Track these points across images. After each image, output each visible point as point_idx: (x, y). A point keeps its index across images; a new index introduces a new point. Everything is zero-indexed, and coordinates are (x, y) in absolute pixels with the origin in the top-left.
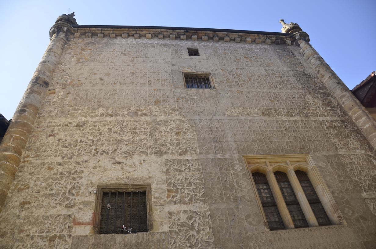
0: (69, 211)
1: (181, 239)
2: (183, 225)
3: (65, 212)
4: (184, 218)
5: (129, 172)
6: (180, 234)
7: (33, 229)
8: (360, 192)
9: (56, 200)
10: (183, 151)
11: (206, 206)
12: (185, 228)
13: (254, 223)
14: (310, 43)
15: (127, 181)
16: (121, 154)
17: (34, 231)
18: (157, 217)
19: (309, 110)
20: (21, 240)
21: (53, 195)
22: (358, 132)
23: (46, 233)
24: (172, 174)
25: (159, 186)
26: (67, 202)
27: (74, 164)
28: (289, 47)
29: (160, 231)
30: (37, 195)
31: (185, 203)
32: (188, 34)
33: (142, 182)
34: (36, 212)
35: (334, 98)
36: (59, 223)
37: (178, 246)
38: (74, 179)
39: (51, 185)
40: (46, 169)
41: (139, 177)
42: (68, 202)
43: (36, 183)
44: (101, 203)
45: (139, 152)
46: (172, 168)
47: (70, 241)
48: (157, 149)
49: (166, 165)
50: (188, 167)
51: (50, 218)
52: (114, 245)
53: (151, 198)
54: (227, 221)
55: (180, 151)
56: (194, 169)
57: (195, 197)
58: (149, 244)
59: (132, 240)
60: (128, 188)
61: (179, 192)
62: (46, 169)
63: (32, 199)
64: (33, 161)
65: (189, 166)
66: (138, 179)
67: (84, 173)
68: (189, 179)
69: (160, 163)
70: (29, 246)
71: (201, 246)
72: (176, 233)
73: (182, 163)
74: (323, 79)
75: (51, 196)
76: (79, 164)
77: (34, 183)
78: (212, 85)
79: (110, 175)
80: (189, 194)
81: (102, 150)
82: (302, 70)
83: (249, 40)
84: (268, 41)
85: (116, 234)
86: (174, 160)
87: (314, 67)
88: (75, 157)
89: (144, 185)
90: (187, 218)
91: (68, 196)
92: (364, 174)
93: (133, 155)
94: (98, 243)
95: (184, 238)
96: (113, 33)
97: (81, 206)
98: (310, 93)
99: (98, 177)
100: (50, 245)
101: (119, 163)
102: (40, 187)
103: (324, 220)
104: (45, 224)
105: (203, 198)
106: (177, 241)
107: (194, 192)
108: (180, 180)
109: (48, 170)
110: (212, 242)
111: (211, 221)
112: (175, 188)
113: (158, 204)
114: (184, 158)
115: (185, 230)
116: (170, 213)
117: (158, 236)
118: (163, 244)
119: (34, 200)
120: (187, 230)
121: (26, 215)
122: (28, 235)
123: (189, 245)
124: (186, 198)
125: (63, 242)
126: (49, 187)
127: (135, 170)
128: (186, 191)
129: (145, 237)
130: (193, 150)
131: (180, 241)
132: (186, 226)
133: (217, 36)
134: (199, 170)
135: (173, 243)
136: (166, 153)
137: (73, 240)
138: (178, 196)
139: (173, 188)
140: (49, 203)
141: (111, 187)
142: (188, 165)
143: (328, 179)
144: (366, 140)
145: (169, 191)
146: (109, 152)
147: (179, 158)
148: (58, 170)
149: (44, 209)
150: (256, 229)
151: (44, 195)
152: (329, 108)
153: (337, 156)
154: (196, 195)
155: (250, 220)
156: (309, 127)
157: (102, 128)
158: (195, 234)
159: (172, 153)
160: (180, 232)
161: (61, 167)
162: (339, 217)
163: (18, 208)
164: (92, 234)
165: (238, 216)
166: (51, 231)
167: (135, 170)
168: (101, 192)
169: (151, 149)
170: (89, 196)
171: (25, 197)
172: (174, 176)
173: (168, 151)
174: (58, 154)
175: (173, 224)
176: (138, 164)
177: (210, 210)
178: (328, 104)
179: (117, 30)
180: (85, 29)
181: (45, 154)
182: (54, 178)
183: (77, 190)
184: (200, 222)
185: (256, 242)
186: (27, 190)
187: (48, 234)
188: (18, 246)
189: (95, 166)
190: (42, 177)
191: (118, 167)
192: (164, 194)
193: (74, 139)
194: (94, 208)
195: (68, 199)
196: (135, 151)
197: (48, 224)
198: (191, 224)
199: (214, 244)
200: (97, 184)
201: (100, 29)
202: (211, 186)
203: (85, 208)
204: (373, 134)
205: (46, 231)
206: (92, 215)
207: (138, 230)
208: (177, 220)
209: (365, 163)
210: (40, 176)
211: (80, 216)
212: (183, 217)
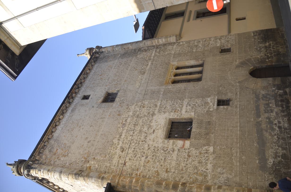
0: (176, 151)
1: (198, 109)
2: (193, 108)
3: (176, 152)
8: (193, 52)
13: (197, 85)
14: (103, 47)
15: (165, 127)
16: (149, 130)
17: (183, 164)
19: (146, 58)
21: (165, 159)
22: (164, 45)
24: (166, 111)
26: (171, 152)
27: (149, 151)
28: (100, 56)
30: (163, 166)
31: (183, 107)
32: (70, 97)
33: (168, 122)
34: (173, 165)
35: (143, 47)
36: (181, 154)
38: (158, 150)
40: (148, 164)
43: (156, 167)
46: (163, 110)
49: (161, 112)
54: (194, 93)
55: (154, 107)
60: (169, 128)
61: (176, 108)
63: (165, 168)
64: (141, 171)
67: (156, 146)
70: (190, 165)
72: (195, 110)
74: (129, 49)
76: (149, 149)
78: (115, 92)
82: (120, 55)
83: (88, 71)
84: (93, 63)
86: (159, 109)
87: (121, 50)
89: (169, 121)
92: (185, 48)
95: (198, 108)
96: (49, 136)
98: (137, 55)
100: (192, 156)
103: (201, 65)
107: (178, 103)
116: (186, 112)
117: (195, 116)
123: (202, 106)
128: (177, 106)
129: (195, 121)
133: (79, 84)
138: (178, 108)
143: (184, 60)
144: (169, 43)
145: (175, 112)
148: (150, 158)
149: (172, 161)
150: (200, 85)
152: (148, 51)
153: (174, 54)
155: (195, 86)
156: (156, 60)
157: (129, 139)
159: (155, 110)
161: (149, 157)
162: (201, 60)
165: (193, 90)
177: (188, 98)
178: (146, 51)
179: (48, 133)
180: (36, 151)
183: (165, 148)
185: (205, 86)
186: (159, 171)
191: (156, 131)
193: (132, 152)
201: (41, 142)
204: (169, 40)
205: (184, 159)
206: (180, 141)
209: (181, 47)
212: (189, 107)
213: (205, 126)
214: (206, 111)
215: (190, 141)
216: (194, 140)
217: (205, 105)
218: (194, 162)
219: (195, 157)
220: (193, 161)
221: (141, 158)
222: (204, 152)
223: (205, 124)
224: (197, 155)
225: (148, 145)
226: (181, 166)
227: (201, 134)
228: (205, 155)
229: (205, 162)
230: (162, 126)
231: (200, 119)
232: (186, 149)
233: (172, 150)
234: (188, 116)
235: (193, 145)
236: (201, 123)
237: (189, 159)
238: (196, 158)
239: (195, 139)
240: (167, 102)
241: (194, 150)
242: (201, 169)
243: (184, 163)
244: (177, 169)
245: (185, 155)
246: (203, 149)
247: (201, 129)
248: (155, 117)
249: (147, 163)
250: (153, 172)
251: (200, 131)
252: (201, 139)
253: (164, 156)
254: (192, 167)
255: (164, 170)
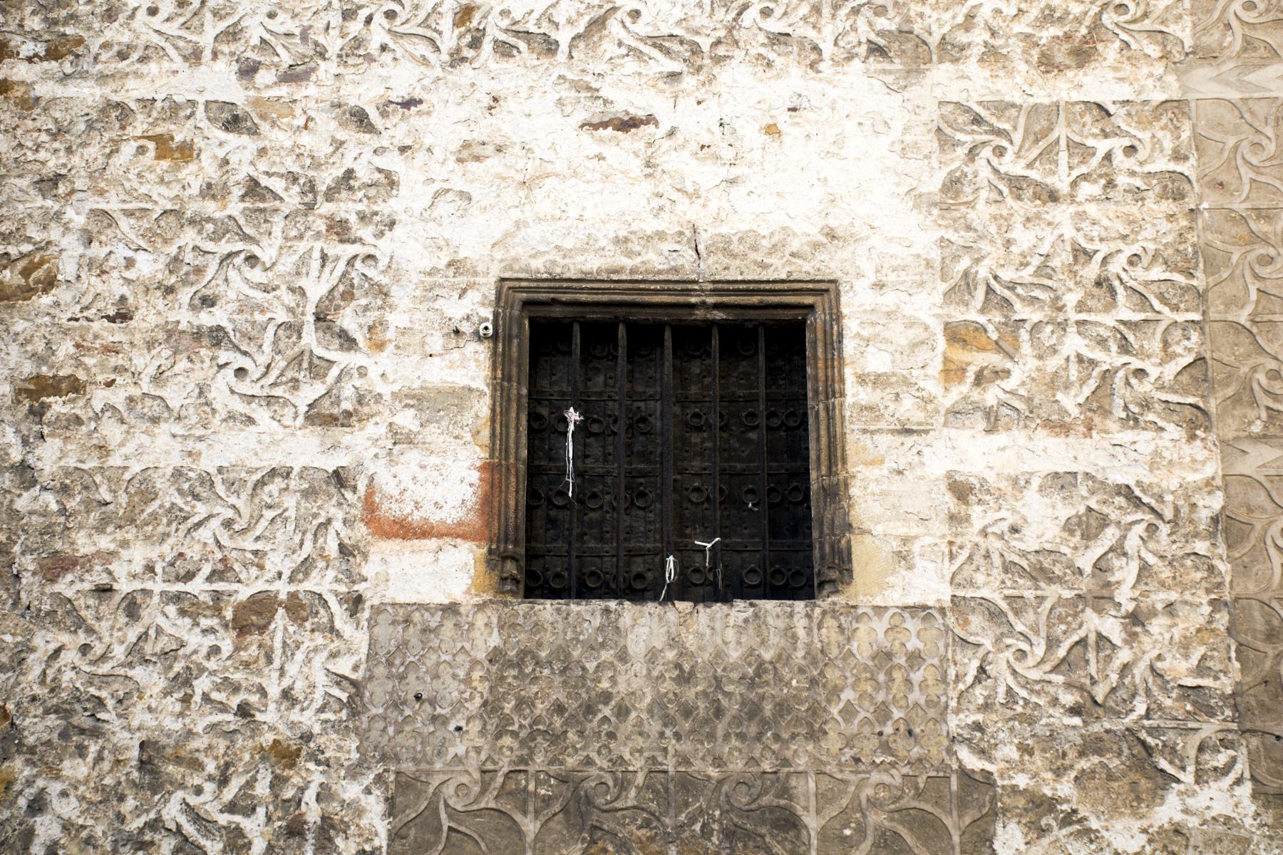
1: (1022, 654)
2: (1040, 571)
3: (308, 451)
4: (1048, 523)
5: (694, 195)
6: (1020, 627)
7: (125, 554)
9: (241, 372)
10: (1068, 37)
11: (1201, 454)
12: (1053, 592)
16: (639, 55)
17: (138, 567)
18: (876, 509)
20: (67, 615)
21: (217, 337)
23: (209, 579)
24: (981, 213)
25: (889, 299)
26: (311, 391)
27: (327, 125)
29: (894, 598)
30: (115, 334)
31: (1061, 427)
33: (778, 270)
34: (130, 448)
37: (1001, 697)
38: (339, 230)
39: (199, 271)
40: (141, 150)
41: (763, 231)
42: (318, 389)
43: (97, 251)
44: (525, 401)
45: (762, 38)
46: (985, 173)
47: (356, 636)
48: (882, 23)
49: (945, 141)
50: (1095, 162)
51: (220, 489)
52: (620, 667)
53: (842, 380)
56: (1138, 182)
57: (1128, 383)
58: (822, 673)
59: (726, 643)
61: (1026, 348)
62: (141, 150)
63: (90, 361)
64: (44, 90)
65: (1108, 157)
66: (755, 248)
67: (403, 190)
68: (1098, 258)
69: (907, 129)
70: (119, 652)
71: (1148, 716)
72: (995, 615)
73: (1061, 131)
75: (206, 341)
76: (360, 119)
77: (81, 250)
79: (573, 212)
80: (1093, 363)
81: (505, 23)
85: (627, 604)
86: (1002, 108)
88: (326, 69)
90: (1068, 528)
91: (319, 351)
93: (718, 60)
94: (524, 653)
95: (1040, 650)
97: (407, 420)
99: (498, 226)
100: (244, 655)
101: (628, 124)
102: (128, 281)
104: (199, 525)
105: (1186, 392)
106: (999, 667)
108: (1036, 261)
109: (158, 157)
110: (1223, 697)
111: (1230, 559)
112: (998, 318)
113: (882, 425)
114: (1075, 97)
115: (1047, 605)
116: (961, 491)
117: (880, 625)
118: (908, 681)
119: (102, 365)
120: (1060, 601)
121: (71, 462)
122: (104, 591)
123: (1069, 699)
124: (1067, 386)
125: (319, 639)
126: (185, 282)
127: (732, 182)
128: (1074, 343)
129: (801, 633)
130: (1147, 24)
131: (1014, 673)
132: (1060, 580)
134: (1173, 187)
135: (969, 679)
136: (950, 50)
137: (376, 630)
138: (1018, 375)
139: (982, 319)
140: (201, 393)
141: (583, 297)
142: (1101, 153)
145: (957, 335)
146: (554, 35)
147: (1042, 97)
148: (226, 162)
149: (178, 429)
151: (161, 336)
154: (1140, 373)
158: (1116, 635)
159: (991, 55)
160: (1017, 613)
161: (245, 139)
163: (8, 418)
164: (487, 597)
166: (237, 567)
167: (732, 182)
168: (521, 326)
169: (842, 22)
170: (447, 350)
171: (40, 346)
172: (993, 229)
173: (962, 38)
174: (206, 40)
175: (979, 560)
176: (751, 135)
177: (1227, 482)
181: (117, 34)
182: (209, 220)
183: (366, 308)
184: (1152, 560)
186: (46, 300)
187: (220, 586)
188: (57, 652)
189: (466, 145)
190: (129, 214)
192: (923, 355)
194: (486, 433)
195: (318, 368)
196: (730, 30)
197: (215, 524)
198: (1088, 569)
199: (1235, 707)
200: (496, 272)
202: (1249, 309)
203: (433, 434)
205: (207, 569)
206: (475, 476)
207: (754, 580)
208: (1001, 537)
210: (112, 204)
211: (406, 478)
212: (1043, 521)
213: (713, 772)
214: (973, 762)
215: (467, 602)
216: (481, 655)
217: (1092, 746)
218: (167, 693)
219: (236, 689)
220: (184, 681)
221: (225, 48)
222: (310, 796)
223: (737, 765)
224: (269, 716)
225: (408, 103)
226: (112, 547)
227: (581, 733)
228: (261, 811)
229: (156, 825)
230: (714, 206)
231: (836, 691)
232: (349, 574)
233: (338, 402)
234: (878, 529)
235: (414, 641)
236: (768, 708)
237: (205, 622)
238: (224, 708)
239: (496, 656)
240: (1137, 194)
241: (344, 666)
242: (64, 794)
243: (150, 569)
244: (72, 504)
245: (269, 575)
246: (354, 772)
247: (667, 721)
248: (860, 85)
249: (151, 145)
250: (33, 232)
251: (623, 712)
252: (507, 740)
253: (258, 317)
254: (91, 679)
255: (65, 348)
